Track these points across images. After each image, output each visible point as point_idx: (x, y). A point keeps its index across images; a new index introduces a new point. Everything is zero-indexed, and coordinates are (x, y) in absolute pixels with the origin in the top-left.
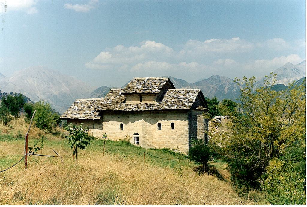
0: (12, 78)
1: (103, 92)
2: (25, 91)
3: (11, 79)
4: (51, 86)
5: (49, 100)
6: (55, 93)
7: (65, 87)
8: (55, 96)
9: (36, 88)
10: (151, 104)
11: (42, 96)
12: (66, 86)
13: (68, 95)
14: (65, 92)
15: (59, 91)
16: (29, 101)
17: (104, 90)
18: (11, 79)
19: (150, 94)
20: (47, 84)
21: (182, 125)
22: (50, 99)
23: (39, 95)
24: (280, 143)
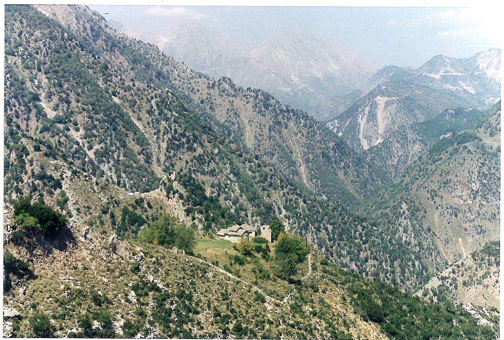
0: (254, 50)
1: (390, 74)
2: (273, 71)
3: (252, 52)
4: (312, 64)
5: (309, 85)
6: (319, 75)
7: (333, 65)
8: (317, 79)
9: (289, 66)
10: (235, 233)
11: (297, 79)
12: (334, 63)
13: (337, 78)
14: (332, 72)
15: (323, 72)
16: (271, 100)
17: (391, 72)
18: (252, 52)
19: (235, 231)
20: (306, 61)
21: (240, 238)
22: (309, 84)
23: (293, 77)
24: (169, 262)
